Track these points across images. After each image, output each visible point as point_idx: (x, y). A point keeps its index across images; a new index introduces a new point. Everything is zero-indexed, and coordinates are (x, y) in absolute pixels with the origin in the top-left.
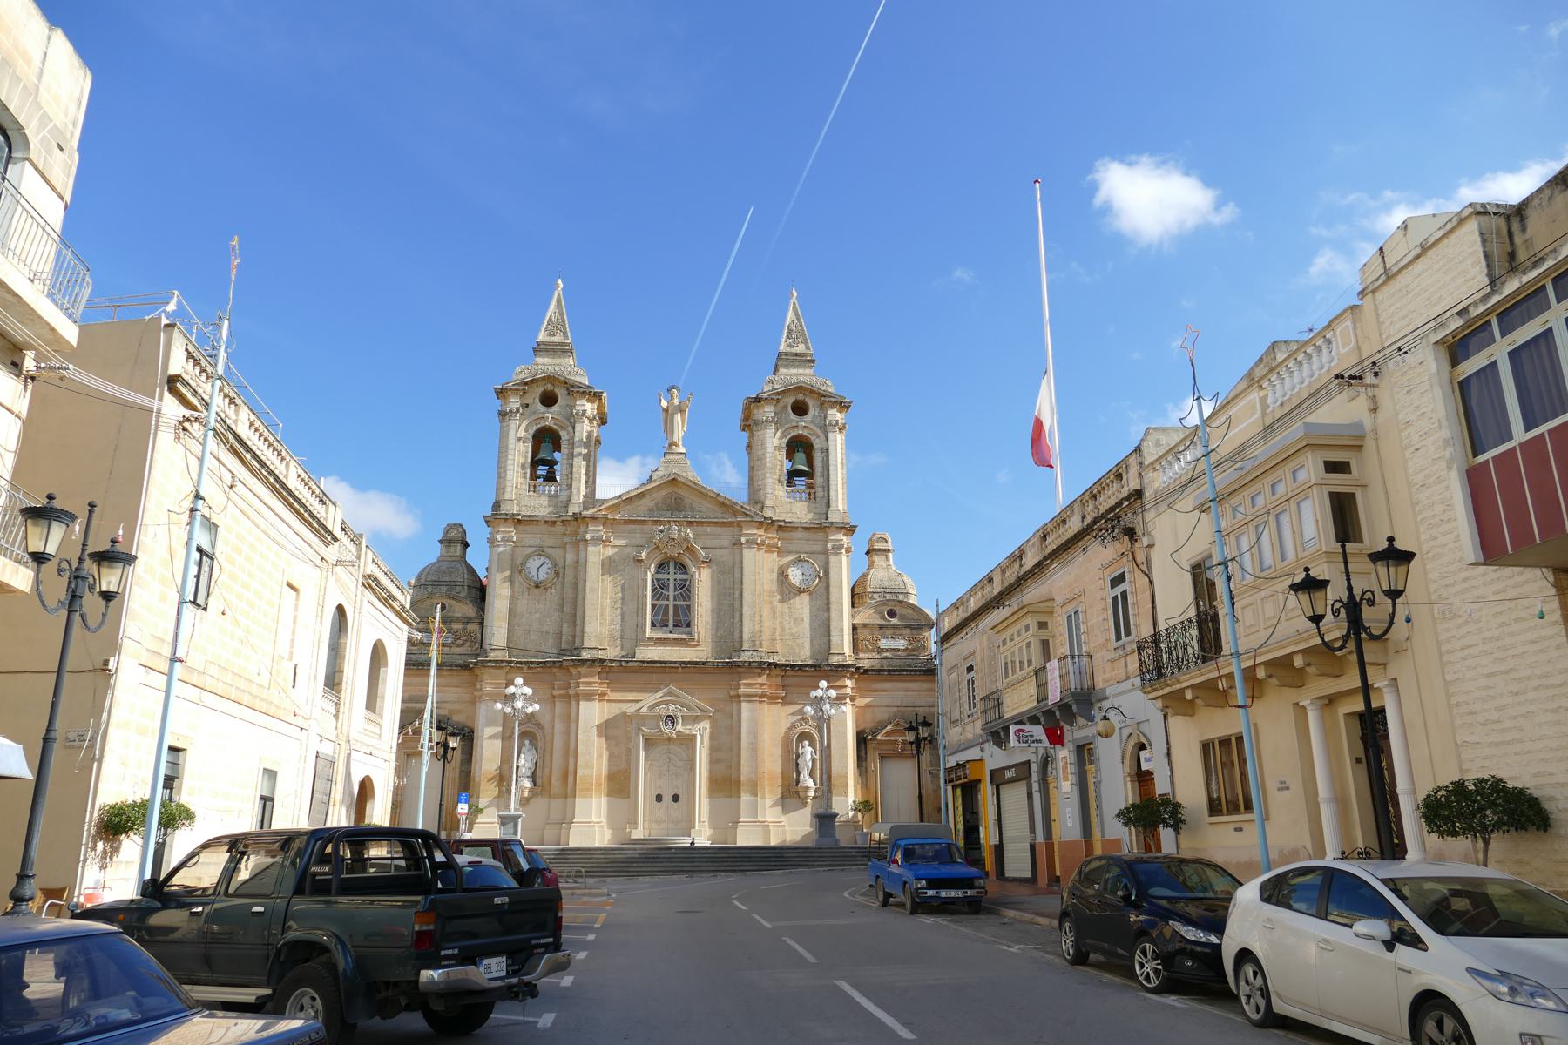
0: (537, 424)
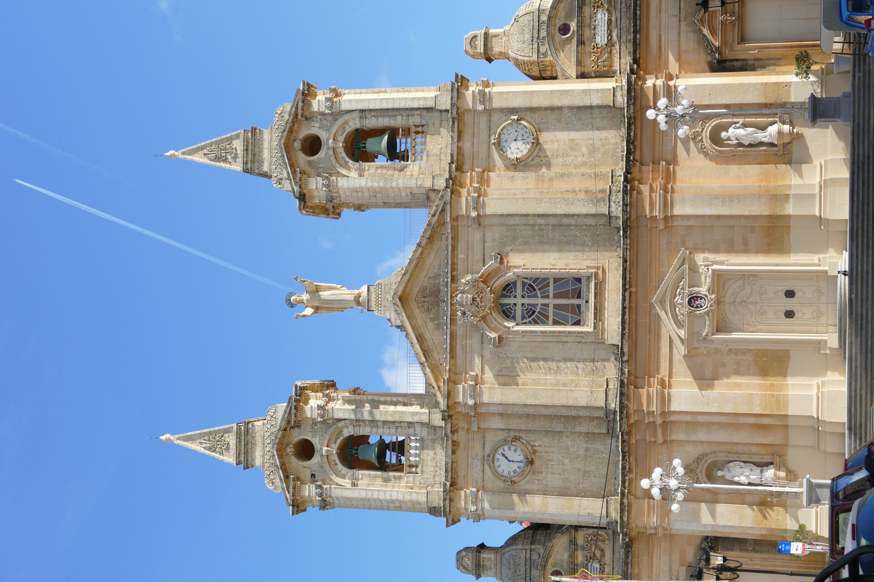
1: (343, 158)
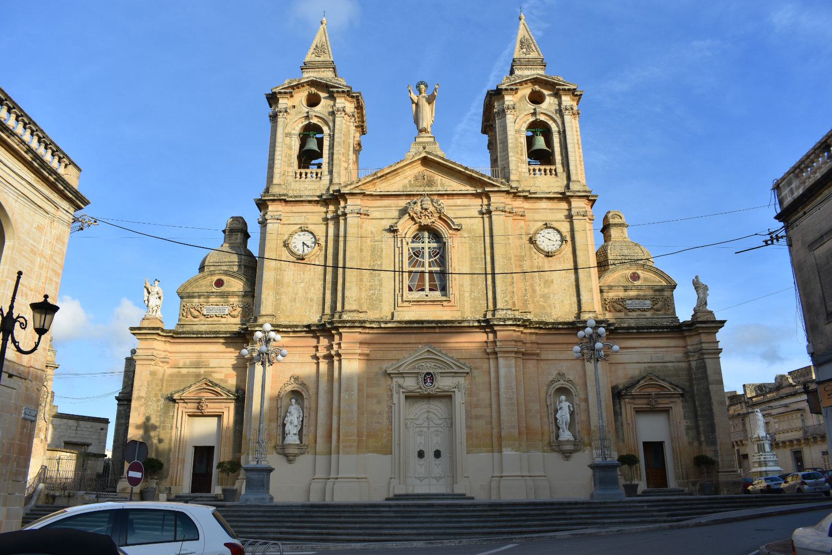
1: (528, 120)
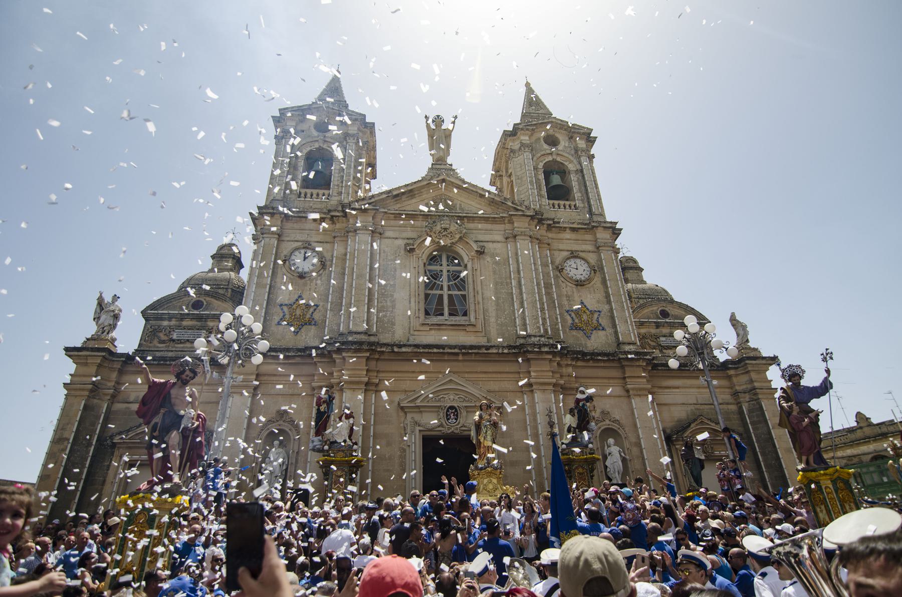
0: (311, 146)
1: (545, 160)
